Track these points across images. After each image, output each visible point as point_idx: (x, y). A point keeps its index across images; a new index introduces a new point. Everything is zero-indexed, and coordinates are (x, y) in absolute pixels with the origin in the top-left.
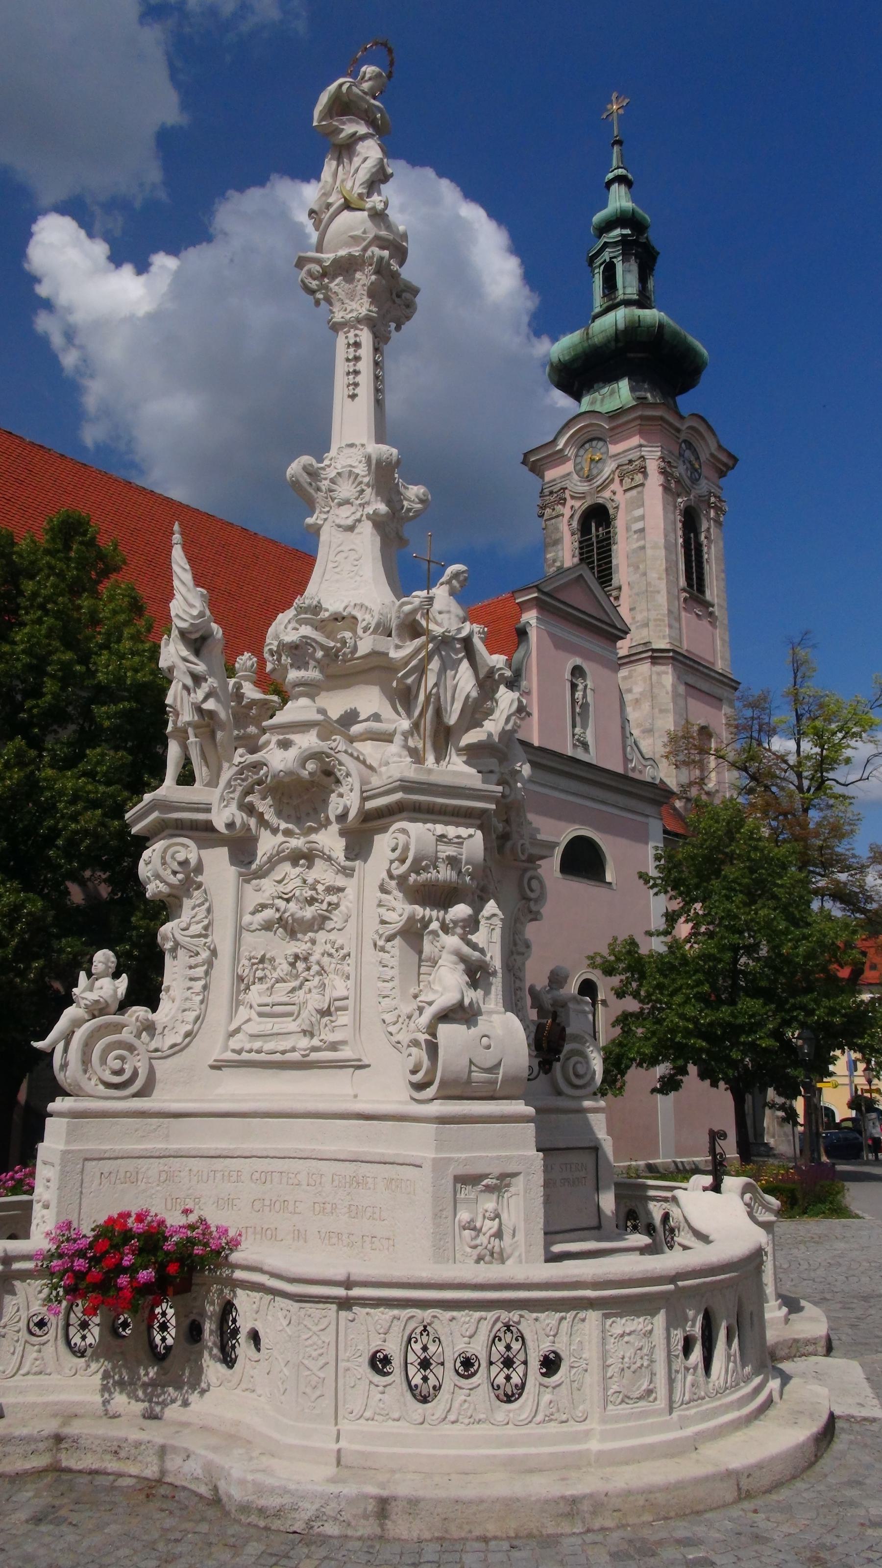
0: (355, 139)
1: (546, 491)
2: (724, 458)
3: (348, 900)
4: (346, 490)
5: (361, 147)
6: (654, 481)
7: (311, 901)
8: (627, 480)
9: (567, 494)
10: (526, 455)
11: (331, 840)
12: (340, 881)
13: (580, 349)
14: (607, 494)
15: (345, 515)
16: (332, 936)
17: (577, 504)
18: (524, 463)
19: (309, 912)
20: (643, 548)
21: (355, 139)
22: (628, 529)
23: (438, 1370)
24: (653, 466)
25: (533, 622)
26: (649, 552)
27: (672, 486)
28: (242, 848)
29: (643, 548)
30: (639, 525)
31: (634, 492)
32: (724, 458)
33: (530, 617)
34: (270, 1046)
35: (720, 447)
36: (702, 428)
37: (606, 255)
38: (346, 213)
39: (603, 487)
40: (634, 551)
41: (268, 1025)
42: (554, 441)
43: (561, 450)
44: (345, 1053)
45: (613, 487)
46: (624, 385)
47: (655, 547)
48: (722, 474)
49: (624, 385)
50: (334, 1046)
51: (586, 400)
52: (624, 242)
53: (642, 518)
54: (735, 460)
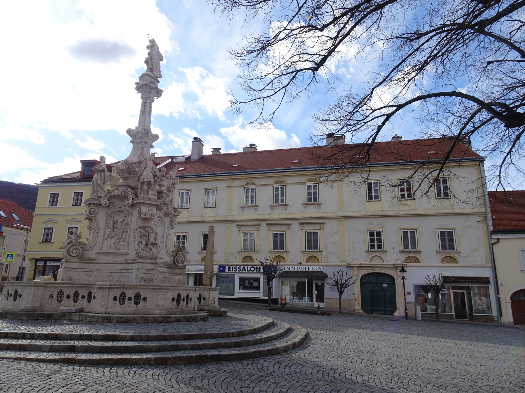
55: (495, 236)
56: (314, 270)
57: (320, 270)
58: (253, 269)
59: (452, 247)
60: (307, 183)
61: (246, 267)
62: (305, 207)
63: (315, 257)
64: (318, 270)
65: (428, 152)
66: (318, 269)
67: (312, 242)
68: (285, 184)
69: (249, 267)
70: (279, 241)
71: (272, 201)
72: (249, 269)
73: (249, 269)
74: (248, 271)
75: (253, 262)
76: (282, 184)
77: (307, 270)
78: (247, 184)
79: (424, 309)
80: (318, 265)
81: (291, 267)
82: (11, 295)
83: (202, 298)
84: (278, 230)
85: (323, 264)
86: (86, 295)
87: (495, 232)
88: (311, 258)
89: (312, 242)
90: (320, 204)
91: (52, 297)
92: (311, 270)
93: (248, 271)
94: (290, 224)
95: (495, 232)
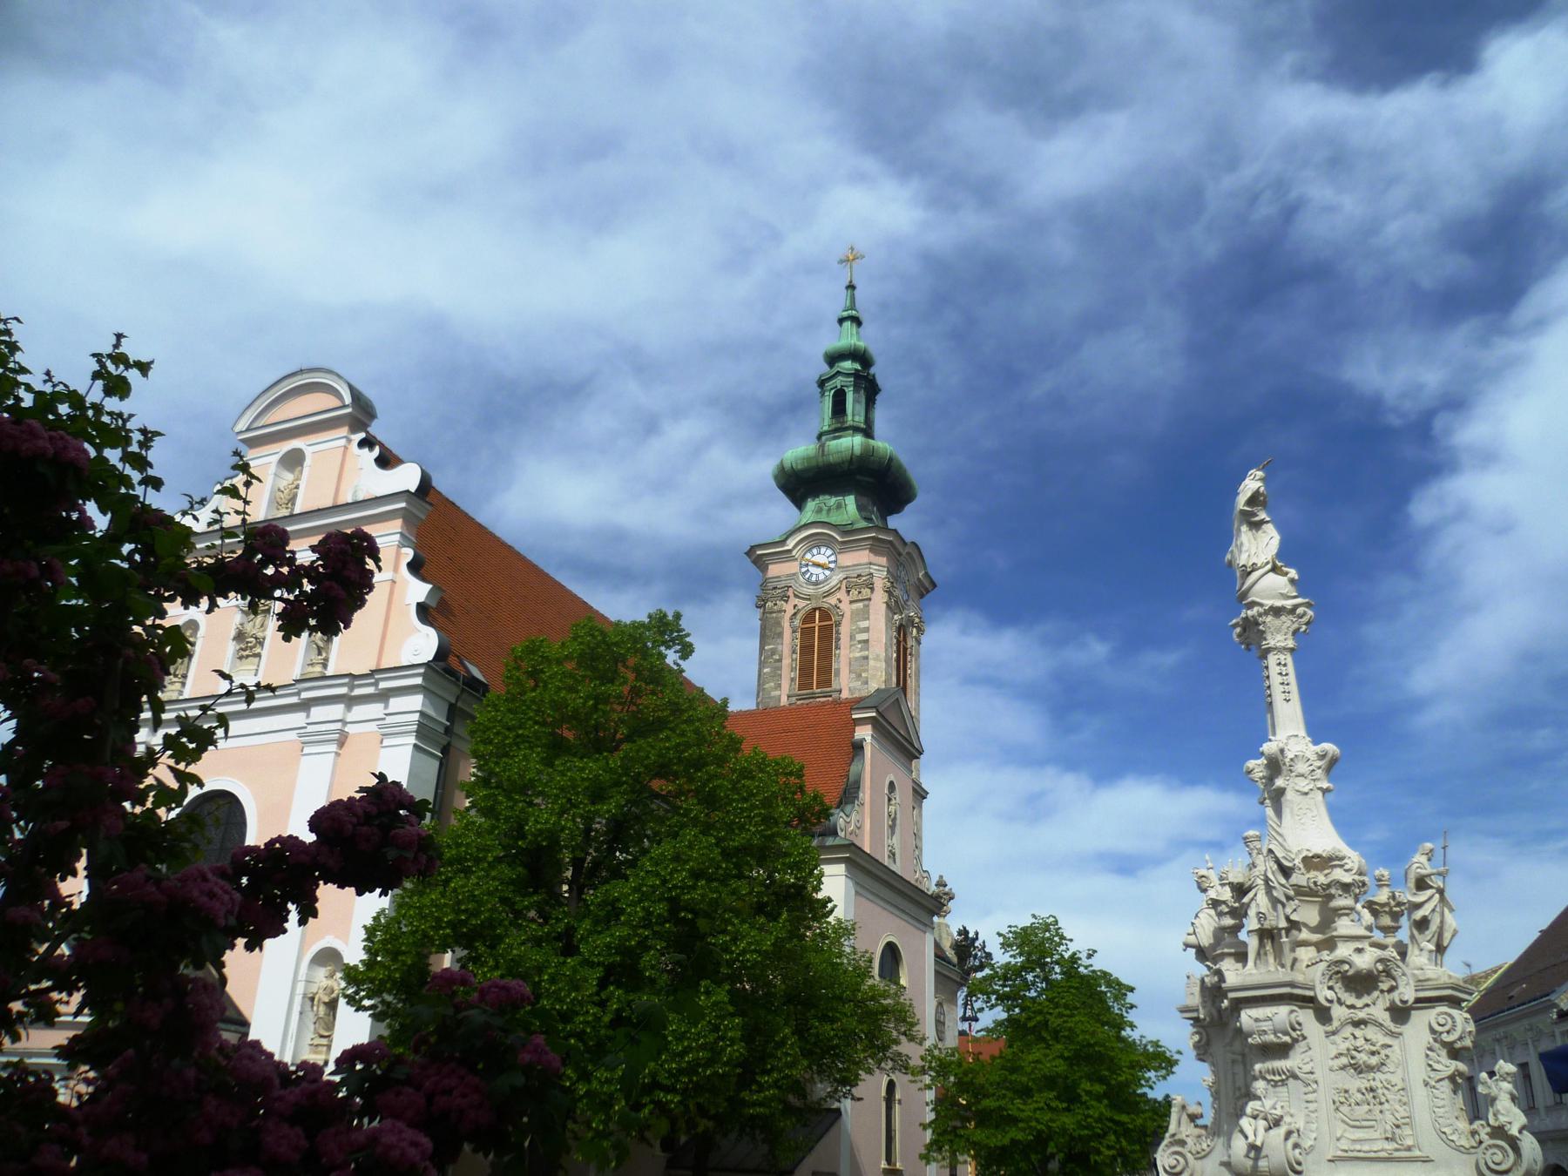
0: (1262, 522)
1: (770, 586)
2: (927, 584)
3: (1395, 1053)
4: (1301, 767)
5: (1265, 527)
6: (879, 599)
7: (1373, 1053)
8: (854, 592)
9: (790, 593)
10: (753, 548)
11: (1379, 1012)
12: (1388, 1041)
13: (814, 463)
14: (832, 600)
15: (1304, 785)
16: (1388, 1076)
17: (801, 604)
18: (748, 554)
19: (1374, 1060)
20: (866, 658)
21: (1262, 522)
22: (852, 637)
24: (880, 581)
25: (869, 739)
26: (872, 663)
27: (894, 607)
28: (1323, 1015)
29: (866, 658)
30: (863, 636)
31: (860, 605)
32: (927, 584)
33: (864, 733)
34: (1366, 1148)
35: (926, 574)
36: (915, 556)
37: (838, 382)
38: (1271, 574)
39: (829, 594)
40: (856, 659)
41: (1360, 1134)
42: (783, 542)
43: (789, 551)
44: (1417, 1153)
45: (838, 595)
46: (850, 501)
47: (877, 658)
48: (922, 596)
49: (850, 501)
50: (1409, 1149)
51: (811, 505)
52: (856, 375)
53: (867, 630)
54: (934, 585)
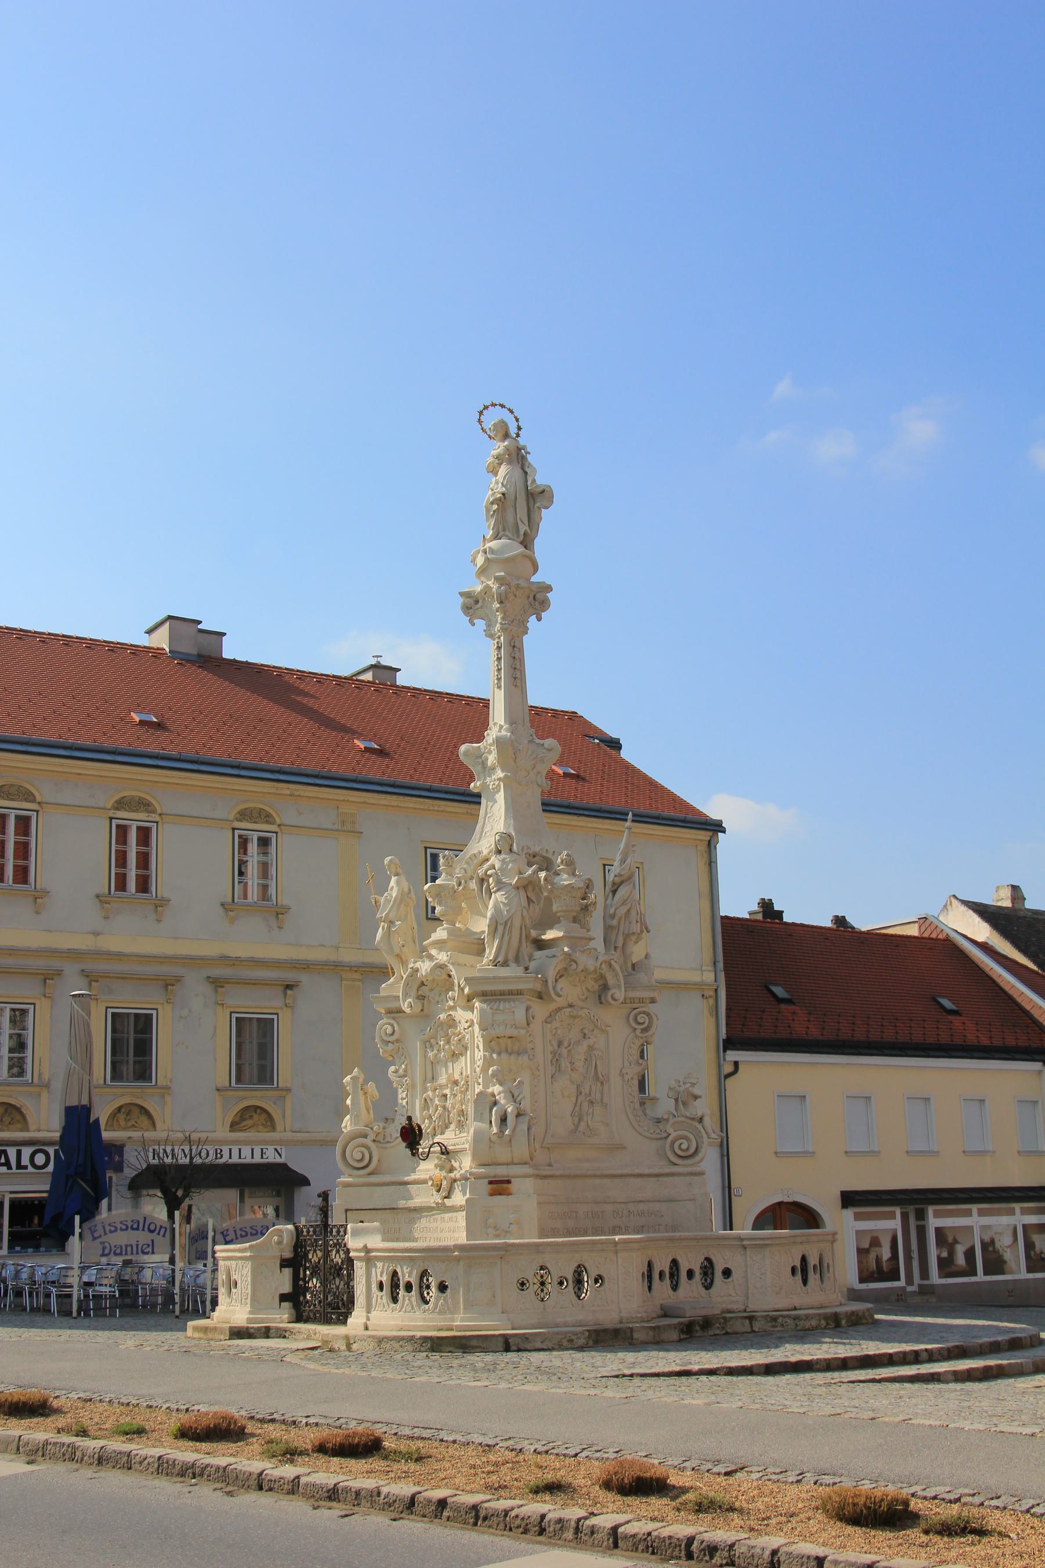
23: (536, 1281)
55: (732, 1055)
56: (257, 1159)
57: (278, 1160)
58: (40, 1159)
59: (143, 1073)
60: (237, 824)
61: (12, 1152)
62: (232, 920)
63: (264, 1111)
64: (271, 1160)
65: (136, 717)
66: (271, 1157)
67: (255, 1049)
68: (155, 817)
69: (26, 1152)
70: (133, 1045)
71: (101, 879)
72: (26, 1161)
73: (26, 1161)
74: (19, 1166)
75: (26, 1129)
76: (142, 816)
77: (235, 1159)
78: (121, 804)
79: (326, 1297)
80: (271, 1142)
81: (271, 1149)
82: (409, 1287)
83: (683, 1274)
84: (255, 1003)
85: (289, 1135)
86: (414, 1280)
87: (730, 1043)
88: (250, 1117)
89: (255, 1049)
90: (161, 904)
91: (523, 1284)
92: (248, 1160)
93: (19, 1166)
94: (178, 979)
95: (730, 1043)
